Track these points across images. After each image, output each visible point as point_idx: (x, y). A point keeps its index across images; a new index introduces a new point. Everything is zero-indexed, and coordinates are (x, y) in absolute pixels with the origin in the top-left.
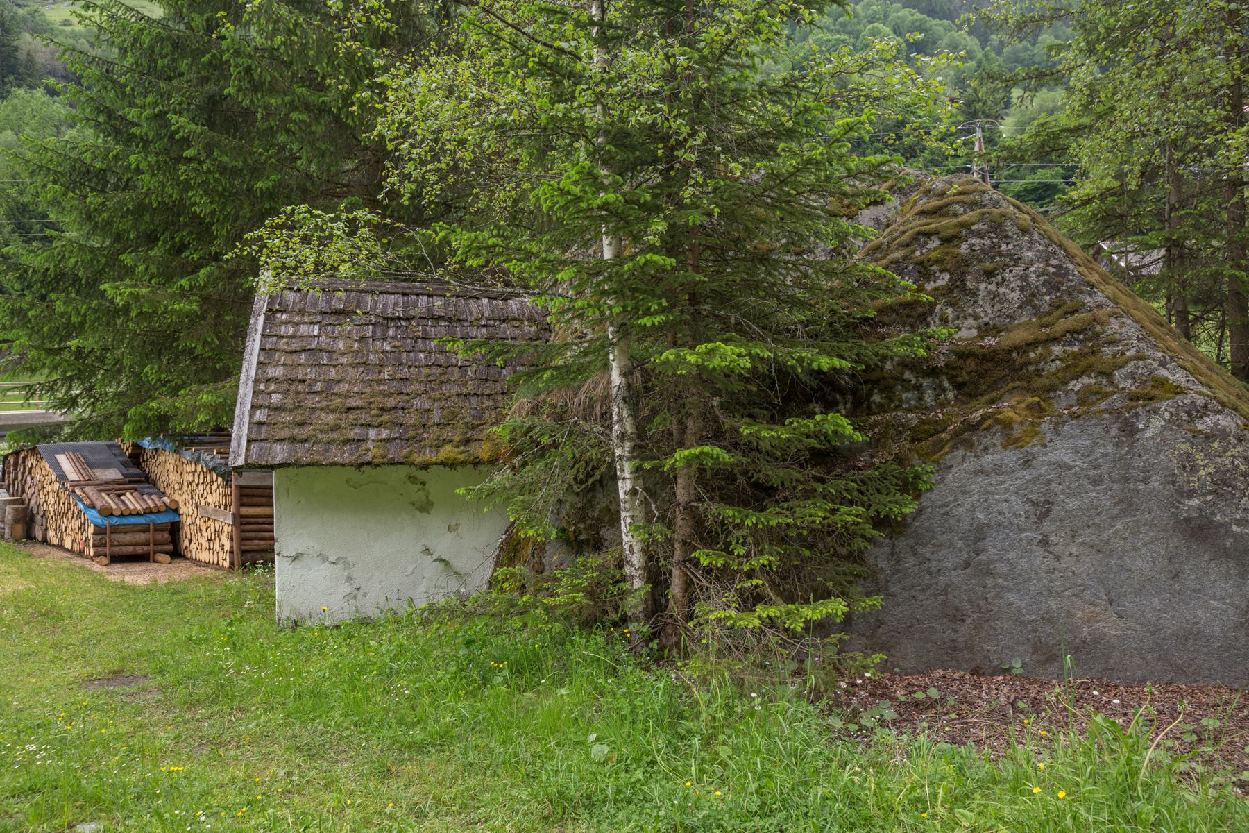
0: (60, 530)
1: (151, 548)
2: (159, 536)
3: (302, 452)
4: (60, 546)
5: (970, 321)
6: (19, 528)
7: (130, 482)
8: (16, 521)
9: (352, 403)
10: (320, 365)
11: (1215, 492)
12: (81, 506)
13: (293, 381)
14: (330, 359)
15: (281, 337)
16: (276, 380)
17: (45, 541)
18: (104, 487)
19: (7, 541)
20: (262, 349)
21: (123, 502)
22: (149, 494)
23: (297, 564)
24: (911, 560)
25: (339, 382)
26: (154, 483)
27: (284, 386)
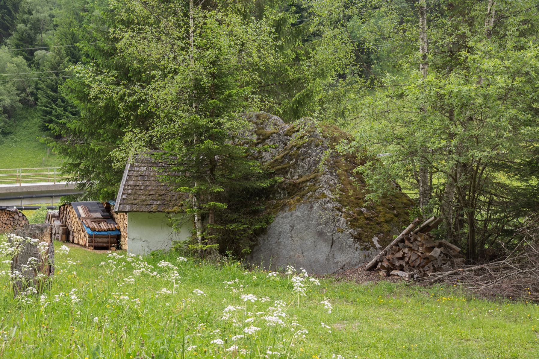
0: (79, 237)
3: (135, 208)
4: (78, 244)
5: (297, 174)
6: (64, 236)
7: (104, 218)
8: (63, 233)
9: (151, 193)
10: (144, 181)
11: (325, 224)
14: (148, 178)
15: (134, 171)
16: (131, 185)
17: (73, 242)
18: (94, 220)
20: (128, 175)
21: (100, 226)
22: (110, 223)
23: (133, 241)
24: (267, 241)
25: (149, 186)
26: (114, 220)
27: (133, 187)
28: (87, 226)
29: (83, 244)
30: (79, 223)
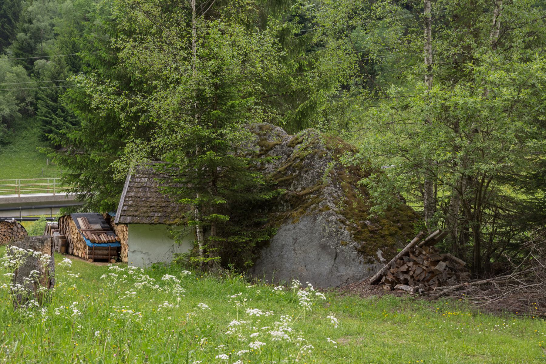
0: (78, 249)
1: (109, 257)
2: (112, 252)
3: (135, 220)
4: (78, 256)
6: (63, 248)
7: (104, 230)
8: (62, 245)
9: (152, 204)
11: (328, 237)
12: (85, 239)
13: (136, 197)
14: (149, 190)
15: (135, 182)
16: (131, 197)
17: (72, 254)
18: (94, 232)
19: (59, 253)
20: (129, 187)
21: (100, 238)
22: (110, 235)
24: (269, 254)
25: (150, 197)
28: (87, 237)
29: (83, 256)
30: (79, 235)
